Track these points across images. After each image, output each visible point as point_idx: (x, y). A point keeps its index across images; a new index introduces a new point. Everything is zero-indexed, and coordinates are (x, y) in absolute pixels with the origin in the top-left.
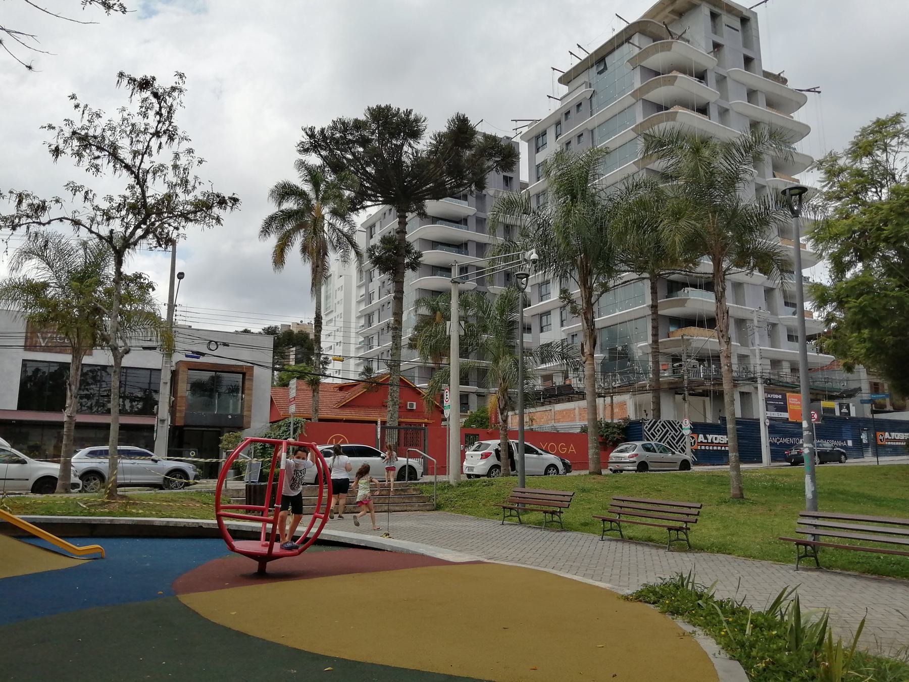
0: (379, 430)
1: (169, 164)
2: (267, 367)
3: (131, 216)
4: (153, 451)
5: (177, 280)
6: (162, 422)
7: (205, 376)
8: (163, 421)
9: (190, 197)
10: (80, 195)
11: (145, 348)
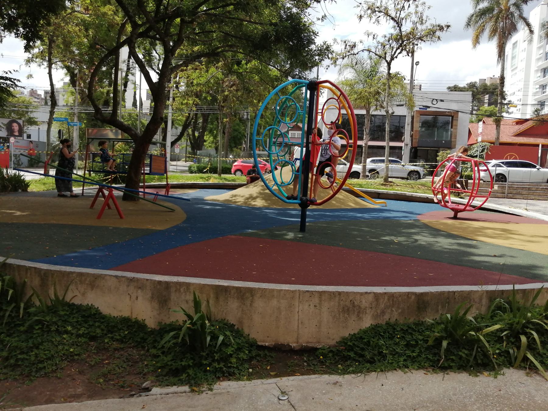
0: (540, 151)
1: (413, 11)
2: (466, 113)
3: (395, 43)
4: (401, 160)
5: (415, 66)
6: (405, 144)
7: (430, 118)
8: (407, 145)
9: (424, 27)
10: (371, 37)
11: (398, 105)
